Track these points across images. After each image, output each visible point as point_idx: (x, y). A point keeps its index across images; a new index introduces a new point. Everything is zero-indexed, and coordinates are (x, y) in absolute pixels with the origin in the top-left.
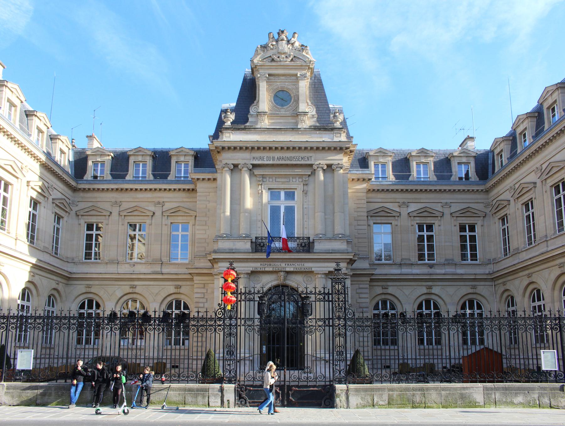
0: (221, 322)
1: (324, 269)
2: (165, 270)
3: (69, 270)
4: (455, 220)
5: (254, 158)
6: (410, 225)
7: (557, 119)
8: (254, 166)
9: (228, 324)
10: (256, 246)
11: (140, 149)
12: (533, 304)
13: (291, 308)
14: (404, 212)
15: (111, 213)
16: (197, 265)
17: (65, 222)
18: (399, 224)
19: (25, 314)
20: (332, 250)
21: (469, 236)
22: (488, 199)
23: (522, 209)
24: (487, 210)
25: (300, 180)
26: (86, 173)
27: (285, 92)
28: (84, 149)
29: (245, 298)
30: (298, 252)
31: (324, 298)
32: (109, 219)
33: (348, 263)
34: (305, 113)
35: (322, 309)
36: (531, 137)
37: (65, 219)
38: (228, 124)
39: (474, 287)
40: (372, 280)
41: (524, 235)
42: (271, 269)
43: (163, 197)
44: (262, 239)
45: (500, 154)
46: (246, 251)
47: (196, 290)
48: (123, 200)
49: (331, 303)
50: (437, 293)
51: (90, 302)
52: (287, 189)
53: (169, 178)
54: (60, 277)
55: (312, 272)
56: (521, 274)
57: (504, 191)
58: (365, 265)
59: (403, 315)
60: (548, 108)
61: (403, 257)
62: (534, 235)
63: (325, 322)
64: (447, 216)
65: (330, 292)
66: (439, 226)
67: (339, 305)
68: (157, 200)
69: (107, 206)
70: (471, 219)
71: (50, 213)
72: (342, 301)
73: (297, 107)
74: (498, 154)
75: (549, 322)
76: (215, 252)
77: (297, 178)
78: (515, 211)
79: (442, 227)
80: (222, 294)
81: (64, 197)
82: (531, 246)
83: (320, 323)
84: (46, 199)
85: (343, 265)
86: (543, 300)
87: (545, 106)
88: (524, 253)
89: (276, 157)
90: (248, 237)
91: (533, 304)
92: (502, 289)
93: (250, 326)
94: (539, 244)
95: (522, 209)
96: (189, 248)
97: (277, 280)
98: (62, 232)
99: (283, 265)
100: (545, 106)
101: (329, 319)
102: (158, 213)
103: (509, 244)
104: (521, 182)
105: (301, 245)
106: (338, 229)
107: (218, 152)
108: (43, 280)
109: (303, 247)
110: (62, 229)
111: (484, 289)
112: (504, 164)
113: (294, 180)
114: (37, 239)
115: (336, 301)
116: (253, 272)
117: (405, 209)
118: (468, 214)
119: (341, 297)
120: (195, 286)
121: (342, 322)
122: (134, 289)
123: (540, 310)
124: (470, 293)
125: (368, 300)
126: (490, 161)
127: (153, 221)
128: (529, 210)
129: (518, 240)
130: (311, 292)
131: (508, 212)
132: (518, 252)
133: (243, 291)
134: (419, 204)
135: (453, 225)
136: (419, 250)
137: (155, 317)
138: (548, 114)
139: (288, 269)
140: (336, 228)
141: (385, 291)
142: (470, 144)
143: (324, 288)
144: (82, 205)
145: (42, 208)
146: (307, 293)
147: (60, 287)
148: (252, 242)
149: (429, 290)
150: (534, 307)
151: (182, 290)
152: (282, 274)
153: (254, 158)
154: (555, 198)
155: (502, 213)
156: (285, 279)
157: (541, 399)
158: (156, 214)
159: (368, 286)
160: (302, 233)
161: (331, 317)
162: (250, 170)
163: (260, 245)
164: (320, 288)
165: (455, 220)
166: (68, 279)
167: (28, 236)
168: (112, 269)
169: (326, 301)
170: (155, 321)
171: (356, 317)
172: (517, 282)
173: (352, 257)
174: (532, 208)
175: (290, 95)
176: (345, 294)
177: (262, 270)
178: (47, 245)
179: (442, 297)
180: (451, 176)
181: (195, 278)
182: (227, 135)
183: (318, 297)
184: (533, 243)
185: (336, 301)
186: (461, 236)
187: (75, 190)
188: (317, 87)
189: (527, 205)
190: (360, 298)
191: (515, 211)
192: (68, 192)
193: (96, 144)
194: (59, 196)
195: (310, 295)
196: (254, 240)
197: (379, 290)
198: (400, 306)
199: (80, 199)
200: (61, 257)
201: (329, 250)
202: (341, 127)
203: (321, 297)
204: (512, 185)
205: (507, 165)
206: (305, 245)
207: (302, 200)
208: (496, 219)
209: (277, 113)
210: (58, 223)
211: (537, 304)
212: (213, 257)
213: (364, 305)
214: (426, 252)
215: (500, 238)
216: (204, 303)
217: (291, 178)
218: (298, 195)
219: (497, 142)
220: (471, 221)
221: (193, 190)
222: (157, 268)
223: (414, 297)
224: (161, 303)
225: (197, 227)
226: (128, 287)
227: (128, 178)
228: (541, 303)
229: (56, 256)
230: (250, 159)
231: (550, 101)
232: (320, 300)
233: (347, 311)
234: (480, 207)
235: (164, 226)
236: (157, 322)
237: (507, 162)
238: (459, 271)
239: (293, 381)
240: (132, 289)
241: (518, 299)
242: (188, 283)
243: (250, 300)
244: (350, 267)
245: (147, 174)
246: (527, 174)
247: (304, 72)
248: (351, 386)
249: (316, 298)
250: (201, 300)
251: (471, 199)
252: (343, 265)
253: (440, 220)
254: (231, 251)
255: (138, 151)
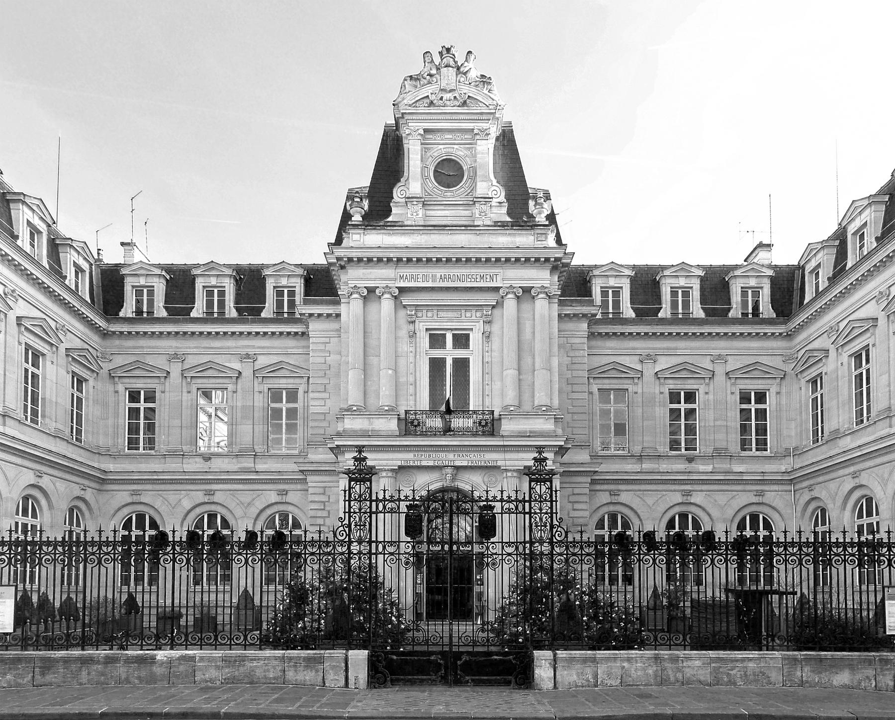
0: (345, 549)
1: (516, 463)
2: (260, 467)
3: (103, 466)
4: (732, 384)
5: (401, 277)
6: (657, 391)
7: (865, 253)
8: (402, 290)
9: (355, 552)
10: (406, 425)
11: (212, 265)
12: (860, 522)
13: (465, 527)
14: (649, 370)
15: (168, 373)
16: (312, 457)
17: (91, 390)
18: (640, 391)
19: (29, 539)
20: (531, 432)
21: (756, 410)
22: (790, 348)
23: (849, 364)
24: (788, 368)
25: (478, 314)
26: (122, 306)
27: (452, 164)
28: (117, 265)
29: (384, 507)
30: (475, 435)
31: (517, 508)
32: (164, 384)
33: (556, 453)
34: (487, 199)
35: (513, 527)
36: (873, 240)
37: (91, 382)
38: (357, 218)
39: (760, 494)
40: (593, 482)
41: (850, 409)
42: (431, 463)
43: (253, 347)
44: (415, 414)
45: (815, 272)
46: (390, 433)
47: (311, 498)
48: (189, 351)
49: (527, 516)
50: (698, 503)
51: (141, 517)
52: (456, 329)
53: (263, 315)
54: (95, 481)
55: (498, 467)
56: (841, 472)
57: (816, 333)
58: (582, 456)
59: (710, 535)
60: (854, 234)
61: (645, 445)
62: (869, 408)
63: (517, 548)
64: (720, 378)
65: (527, 498)
66: (707, 393)
67: (541, 519)
68: (244, 351)
69: (161, 362)
70: (760, 381)
71: (63, 372)
72: (546, 513)
73: (473, 189)
74: (811, 272)
75: (885, 550)
76: (339, 435)
77: (474, 312)
78: (838, 367)
79: (711, 397)
80: (345, 501)
81: (87, 347)
82: (862, 426)
83: (510, 550)
84: (54, 349)
85: (549, 455)
86: (877, 514)
87: (851, 229)
88: (849, 437)
89: (438, 276)
90: (393, 410)
91: (860, 522)
92: (806, 497)
93: (391, 554)
94: (875, 422)
95: (849, 364)
96: (300, 429)
97: (441, 480)
98: (87, 406)
99: (451, 456)
100: (851, 229)
101: (525, 542)
102: (247, 373)
103: (822, 422)
104: (851, 318)
105: (480, 423)
106: (541, 398)
107: (342, 267)
108: (58, 484)
109: (483, 426)
110: (87, 399)
111: (775, 497)
112: (821, 289)
113: (468, 314)
114: (43, 416)
115: (535, 513)
116: (400, 467)
117: (650, 365)
118: (756, 374)
119: (546, 507)
120: (311, 490)
121: (546, 548)
122: (211, 497)
123: (872, 532)
124: (753, 503)
125: (587, 514)
126: (797, 285)
127: (239, 387)
128: (861, 366)
129: (839, 416)
130: (495, 497)
131: (824, 370)
132: (836, 435)
133: (381, 497)
134: (673, 357)
135: (729, 392)
136: (672, 433)
137: (100, 541)
138: (854, 244)
139: (458, 463)
140: (537, 395)
141: (615, 499)
142: (762, 257)
143: (517, 491)
144: (119, 361)
145: (48, 363)
146: (487, 500)
147: (89, 495)
148: (399, 419)
149: (685, 498)
150: (861, 527)
151: (291, 498)
152: (449, 470)
153: (401, 277)
154: (855, 373)
155: (813, 373)
156: (454, 479)
157: (879, 678)
158: (243, 374)
159: (587, 491)
160: (481, 403)
161: (374, 516)
162: (396, 297)
163: (412, 423)
164: (510, 492)
165: (732, 384)
166: (102, 481)
167: (26, 411)
168: (173, 465)
169: (520, 513)
170: (173, 548)
171: (570, 539)
172: (832, 486)
173: (563, 443)
174: (868, 361)
175: (461, 168)
176: (552, 501)
177: (417, 463)
178: (61, 427)
179: (708, 509)
180: (729, 310)
181: (309, 478)
182: (356, 237)
183: (507, 506)
184: (865, 421)
185: (535, 513)
186: (742, 410)
187: (105, 335)
188: (507, 143)
189: (858, 357)
190: (574, 510)
191: (838, 367)
192: (94, 339)
193: (137, 257)
194: (78, 344)
195: (493, 504)
196: (403, 416)
197: (604, 498)
198: (765, 507)
199: (114, 351)
200: (87, 446)
201: (526, 432)
202: (547, 223)
203: (512, 506)
204: (833, 323)
205: (826, 290)
206: (487, 423)
207: (481, 347)
208: (803, 381)
209: (440, 199)
210: (80, 390)
211: (865, 521)
212: (337, 443)
213: (581, 521)
214: (683, 437)
215: (808, 414)
216: (324, 517)
217: (463, 311)
218: (475, 339)
219: (811, 250)
220: (759, 385)
221: (303, 334)
222: (248, 463)
223: (662, 508)
224: (256, 520)
225: (311, 395)
226: (200, 494)
227: (194, 314)
228: (874, 520)
229: (78, 444)
230: (395, 280)
231: (857, 223)
232: (509, 511)
233: (555, 530)
234: (777, 362)
235: (256, 394)
236: (236, 548)
237: (827, 284)
238: (738, 468)
239: (465, 645)
240: (208, 497)
241: (833, 513)
242: (299, 487)
243: (392, 511)
244: (559, 459)
245: (227, 308)
246: (863, 303)
247: (484, 125)
248: (561, 654)
249: (502, 507)
250: (320, 514)
251: (762, 348)
252: (549, 455)
253: (708, 384)
254: (365, 434)
255: (211, 266)
